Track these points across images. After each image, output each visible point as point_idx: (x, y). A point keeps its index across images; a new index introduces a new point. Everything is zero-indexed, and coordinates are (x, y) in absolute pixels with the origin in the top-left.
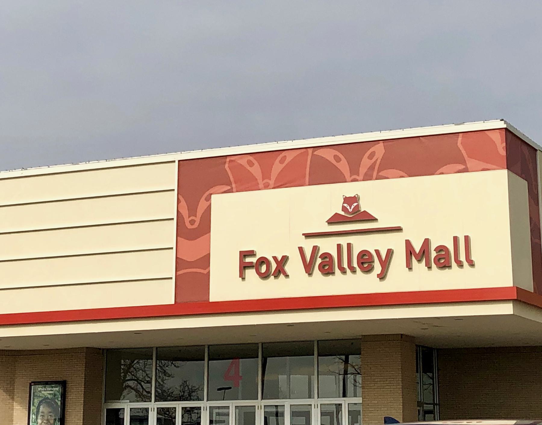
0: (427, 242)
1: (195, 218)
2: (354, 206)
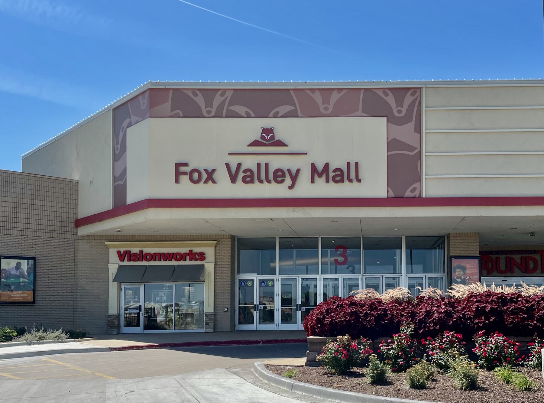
0: (327, 165)
1: (329, 106)
2: (270, 135)
